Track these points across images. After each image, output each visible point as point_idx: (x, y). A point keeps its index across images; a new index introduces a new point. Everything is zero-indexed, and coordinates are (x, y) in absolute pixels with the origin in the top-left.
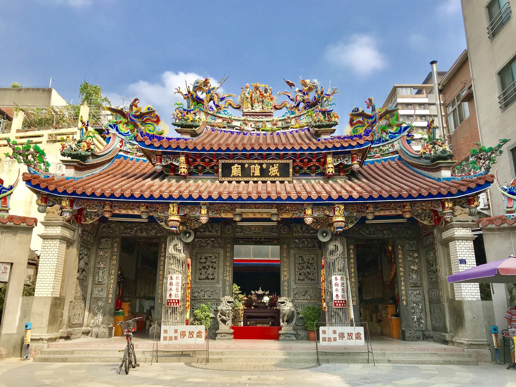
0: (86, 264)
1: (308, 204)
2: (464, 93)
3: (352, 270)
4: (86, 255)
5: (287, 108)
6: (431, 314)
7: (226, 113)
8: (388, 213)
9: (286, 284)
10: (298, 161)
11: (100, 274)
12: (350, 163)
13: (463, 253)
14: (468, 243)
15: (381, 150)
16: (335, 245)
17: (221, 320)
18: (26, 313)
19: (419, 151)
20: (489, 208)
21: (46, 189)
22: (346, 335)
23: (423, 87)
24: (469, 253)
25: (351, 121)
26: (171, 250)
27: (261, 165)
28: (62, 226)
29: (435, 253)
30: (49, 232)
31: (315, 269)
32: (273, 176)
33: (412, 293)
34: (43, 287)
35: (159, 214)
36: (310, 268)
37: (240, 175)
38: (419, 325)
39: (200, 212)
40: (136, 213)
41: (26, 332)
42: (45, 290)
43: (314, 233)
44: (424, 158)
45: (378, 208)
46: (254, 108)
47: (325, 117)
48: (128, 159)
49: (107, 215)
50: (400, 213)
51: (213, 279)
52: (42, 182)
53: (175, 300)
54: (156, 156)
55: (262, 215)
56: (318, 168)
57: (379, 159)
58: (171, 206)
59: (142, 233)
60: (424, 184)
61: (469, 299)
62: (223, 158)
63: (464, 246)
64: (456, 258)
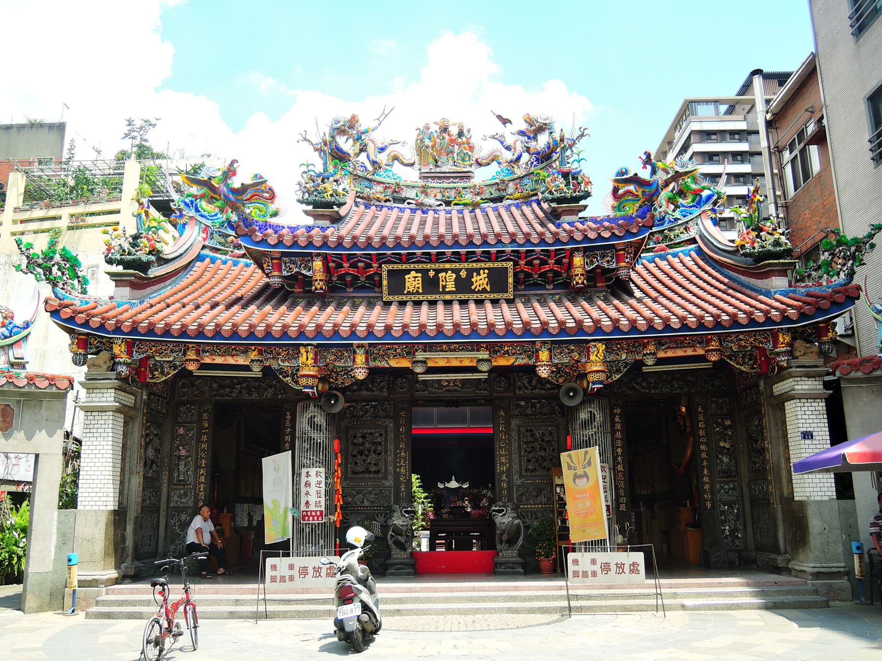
0: (157, 451)
1: (544, 343)
2: (811, 129)
4: (156, 435)
5: (499, 163)
6: (753, 522)
7: (390, 174)
8: (680, 353)
9: (504, 477)
10: (522, 262)
11: (182, 467)
12: (614, 266)
13: (808, 421)
14: (816, 404)
15: (666, 237)
16: (591, 412)
17: (394, 543)
18: (66, 538)
19: (733, 241)
20: (853, 334)
21: (86, 324)
22: (613, 567)
23: (738, 102)
24: (818, 421)
25: (615, 191)
26: (302, 424)
27: (457, 271)
28: (116, 389)
29: (760, 420)
31: (554, 450)
32: (479, 292)
33: (722, 488)
34: (91, 494)
35: (281, 363)
36: (545, 450)
37: (421, 291)
38: (733, 542)
39: (354, 361)
40: (241, 361)
41: (70, 569)
42: (95, 499)
43: (552, 389)
44: (742, 255)
45: (663, 345)
46: (439, 164)
47: (568, 184)
48: (219, 261)
49: (192, 367)
50: (700, 352)
51: (377, 472)
52: (79, 313)
53: (316, 511)
54: (272, 259)
55: (461, 362)
57: (663, 252)
58: (302, 350)
59: (249, 394)
60: (742, 301)
61: (818, 498)
62: (389, 262)
63: (810, 408)
64: (797, 430)
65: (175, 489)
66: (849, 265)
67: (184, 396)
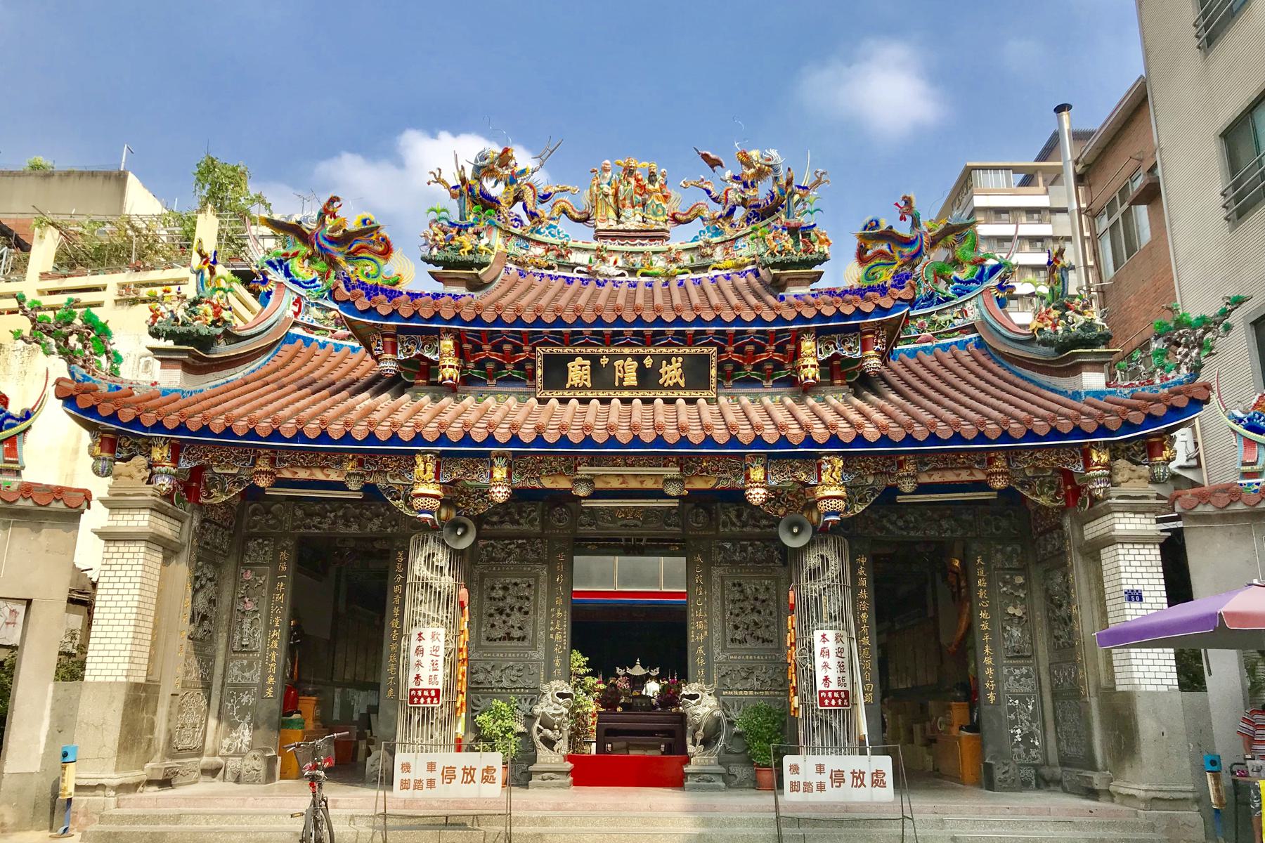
0: (212, 602)
1: (756, 456)
2: (1139, 184)
3: (864, 616)
4: (211, 580)
5: (703, 219)
6: (1056, 724)
8: (950, 477)
9: (701, 650)
11: (246, 626)
12: (858, 355)
14: (1146, 552)
15: (934, 322)
16: (822, 557)
17: (542, 739)
18: (63, 723)
19: (1026, 326)
20: (1199, 466)
21: (114, 418)
22: (848, 777)
23: (1037, 169)
24: (1150, 576)
25: (861, 252)
26: (418, 567)
27: (639, 358)
28: (152, 509)
29: (1065, 575)
30: (120, 523)
31: (771, 613)
32: (669, 388)
33: (1011, 673)
34: (106, 660)
36: (759, 612)
37: (589, 384)
38: (1027, 752)
39: (491, 475)
40: (334, 476)
41: (64, 768)
42: (110, 666)
44: (1039, 343)
45: (926, 465)
46: (622, 219)
47: (796, 243)
48: (314, 344)
49: (263, 482)
50: (980, 476)
51: (524, 638)
53: (429, 690)
54: (384, 336)
55: (642, 482)
56: (779, 366)
57: (928, 344)
58: (419, 459)
59: (347, 526)
61: (1150, 688)
62: (546, 344)
63: (1138, 558)
64: (1118, 588)
65: (236, 658)
66: (1194, 354)
67: (255, 527)
